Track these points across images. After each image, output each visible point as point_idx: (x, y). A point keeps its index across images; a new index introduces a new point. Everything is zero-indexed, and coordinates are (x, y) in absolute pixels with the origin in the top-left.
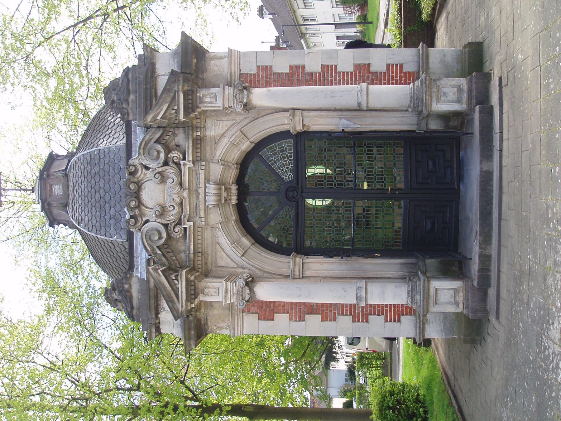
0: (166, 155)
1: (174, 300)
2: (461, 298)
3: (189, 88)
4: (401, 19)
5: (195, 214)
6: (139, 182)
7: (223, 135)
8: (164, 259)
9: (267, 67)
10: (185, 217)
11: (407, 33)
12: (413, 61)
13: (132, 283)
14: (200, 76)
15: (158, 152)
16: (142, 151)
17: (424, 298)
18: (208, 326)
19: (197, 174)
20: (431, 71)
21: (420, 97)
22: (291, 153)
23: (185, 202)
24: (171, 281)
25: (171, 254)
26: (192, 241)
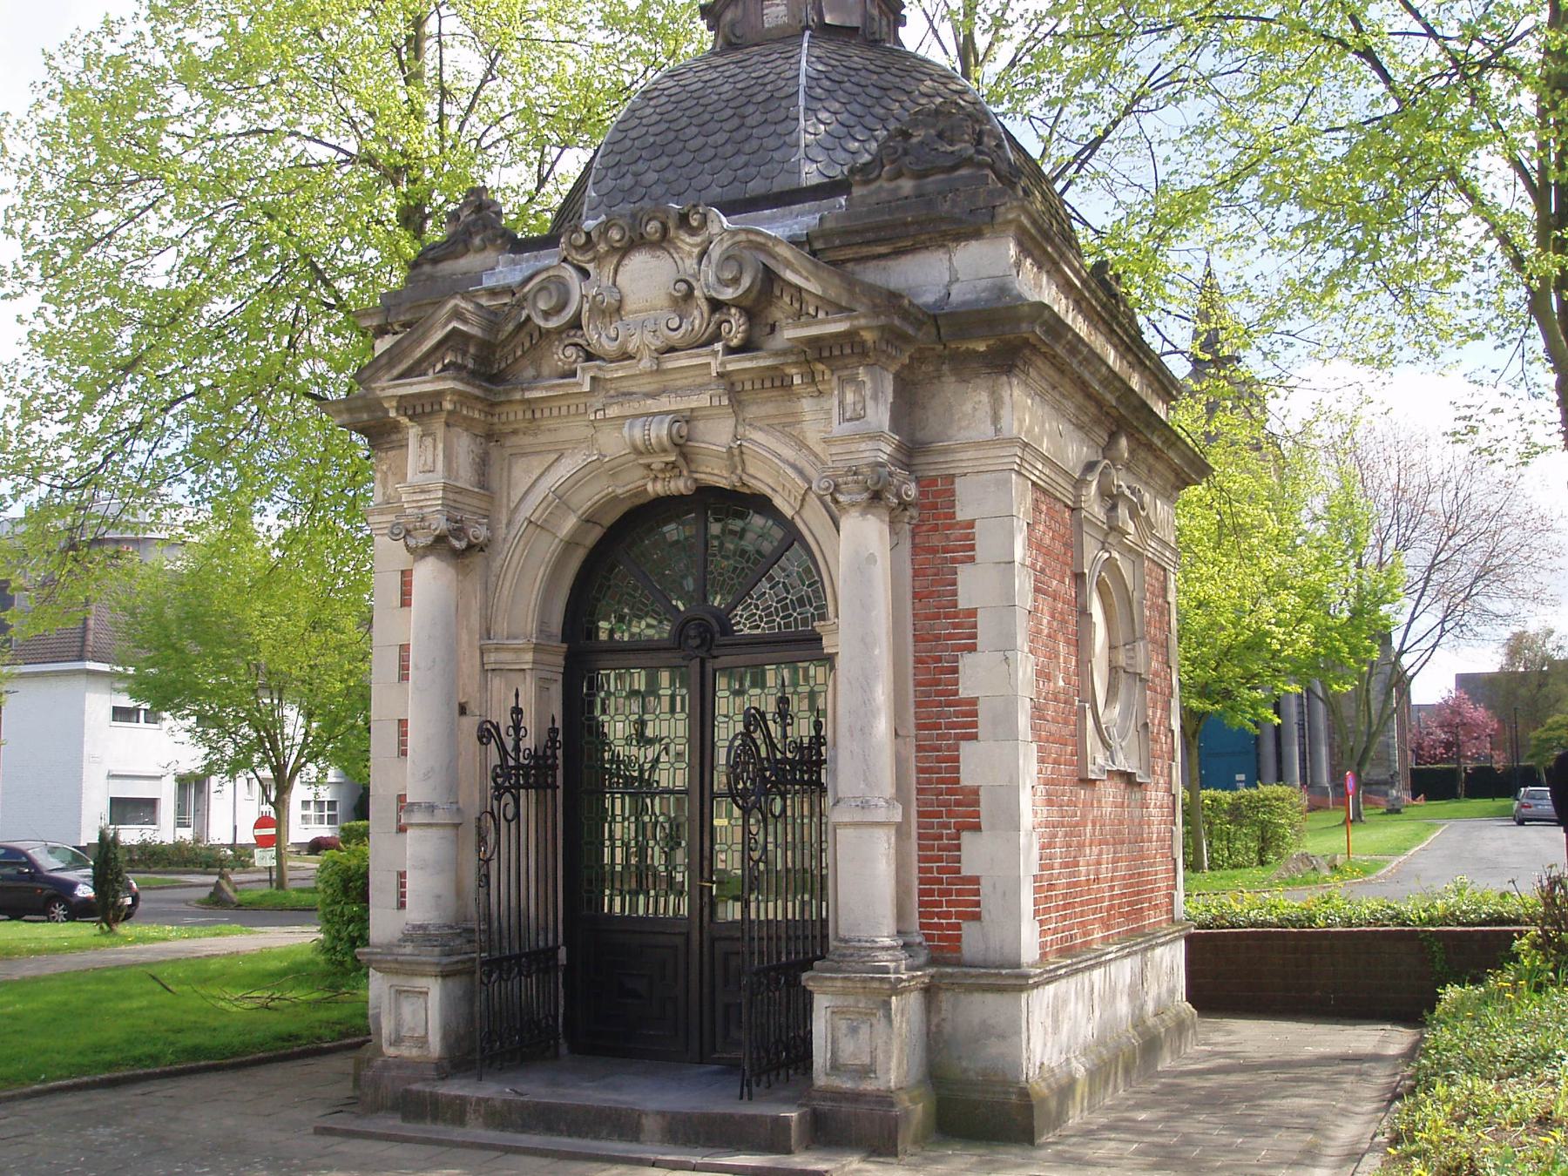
0: (735, 303)
1: (394, 367)
2: (408, 1051)
3: (870, 343)
4: (1473, 925)
5: (612, 392)
6: (671, 241)
7: (802, 444)
8: (510, 327)
9: (972, 548)
10: (600, 368)
11: (1422, 939)
12: (987, 949)
13: (486, 253)
14: (945, 367)
15: (736, 281)
16: (742, 237)
17: (402, 963)
18: (388, 450)
19: (701, 388)
20: (962, 996)
21: (844, 966)
22: (796, 627)
23: (630, 367)
24: (439, 354)
25: (527, 345)
26: (551, 394)
